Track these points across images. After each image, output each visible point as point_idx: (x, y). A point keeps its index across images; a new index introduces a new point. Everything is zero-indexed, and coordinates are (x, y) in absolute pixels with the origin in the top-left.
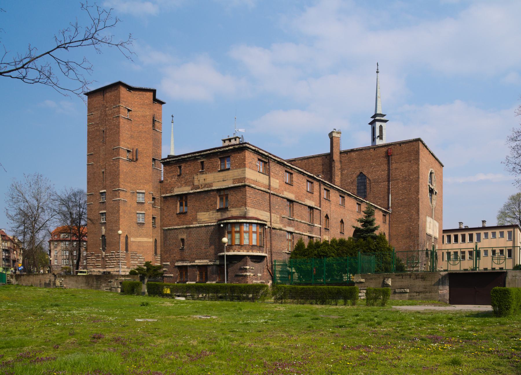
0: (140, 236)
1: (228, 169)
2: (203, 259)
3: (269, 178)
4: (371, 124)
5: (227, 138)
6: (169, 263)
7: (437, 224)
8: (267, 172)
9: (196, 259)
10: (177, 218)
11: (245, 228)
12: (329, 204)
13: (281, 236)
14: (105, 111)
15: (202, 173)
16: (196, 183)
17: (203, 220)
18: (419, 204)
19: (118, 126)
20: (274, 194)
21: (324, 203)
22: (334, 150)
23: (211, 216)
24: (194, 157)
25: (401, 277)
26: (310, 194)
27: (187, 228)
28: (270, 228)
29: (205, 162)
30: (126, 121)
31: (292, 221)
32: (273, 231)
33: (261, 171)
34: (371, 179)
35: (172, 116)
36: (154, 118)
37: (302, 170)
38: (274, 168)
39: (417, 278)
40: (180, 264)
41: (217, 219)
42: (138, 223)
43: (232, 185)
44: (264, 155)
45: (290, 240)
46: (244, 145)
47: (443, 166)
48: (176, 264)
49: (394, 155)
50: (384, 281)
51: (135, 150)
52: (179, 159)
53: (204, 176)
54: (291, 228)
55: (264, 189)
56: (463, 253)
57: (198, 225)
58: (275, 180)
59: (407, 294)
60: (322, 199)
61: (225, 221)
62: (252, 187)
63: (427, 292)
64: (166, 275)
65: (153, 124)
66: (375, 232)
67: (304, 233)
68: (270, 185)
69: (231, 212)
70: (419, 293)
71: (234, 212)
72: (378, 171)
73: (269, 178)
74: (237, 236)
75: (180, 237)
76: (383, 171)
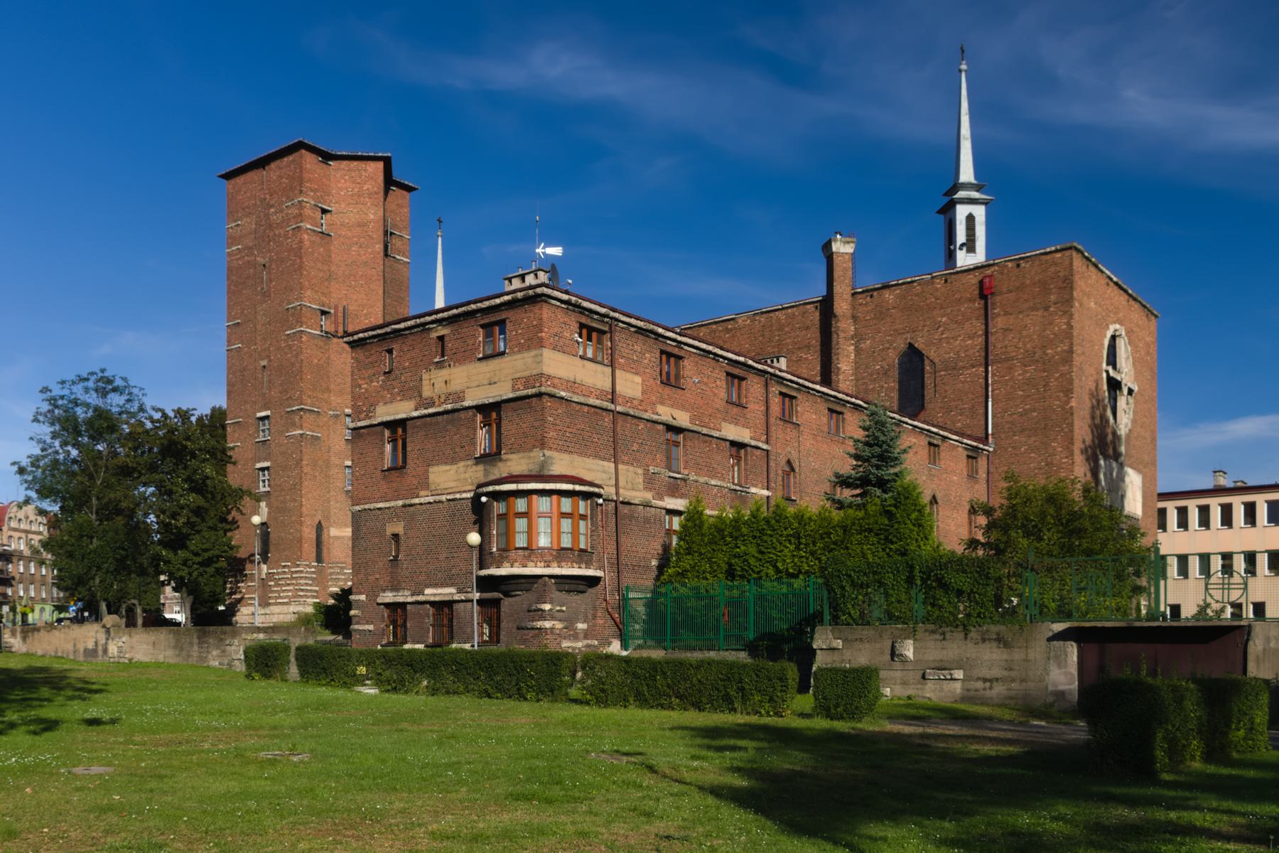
1: (503, 354)
2: (442, 585)
6: (363, 597)
10: (382, 482)
13: (647, 520)
14: (267, 216)
15: (440, 365)
16: (427, 392)
17: (442, 486)
18: (1072, 424)
19: (298, 252)
21: (778, 430)
23: (462, 476)
26: (736, 410)
27: (404, 506)
30: (317, 239)
32: (624, 510)
33: (590, 355)
34: (936, 361)
36: (385, 226)
37: (710, 348)
38: (630, 347)
39: (984, 640)
40: (388, 597)
41: (476, 482)
43: (511, 395)
44: (597, 313)
46: (539, 290)
49: (1001, 293)
50: (893, 647)
51: (341, 309)
53: (444, 373)
55: (597, 402)
56: (1227, 557)
57: (431, 499)
58: (629, 376)
61: (490, 488)
62: (562, 398)
63: (1013, 680)
70: (990, 681)
71: (516, 463)
72: (955, 338)
74: (521, 524)
75: (391, 529)
76: (970, 338)
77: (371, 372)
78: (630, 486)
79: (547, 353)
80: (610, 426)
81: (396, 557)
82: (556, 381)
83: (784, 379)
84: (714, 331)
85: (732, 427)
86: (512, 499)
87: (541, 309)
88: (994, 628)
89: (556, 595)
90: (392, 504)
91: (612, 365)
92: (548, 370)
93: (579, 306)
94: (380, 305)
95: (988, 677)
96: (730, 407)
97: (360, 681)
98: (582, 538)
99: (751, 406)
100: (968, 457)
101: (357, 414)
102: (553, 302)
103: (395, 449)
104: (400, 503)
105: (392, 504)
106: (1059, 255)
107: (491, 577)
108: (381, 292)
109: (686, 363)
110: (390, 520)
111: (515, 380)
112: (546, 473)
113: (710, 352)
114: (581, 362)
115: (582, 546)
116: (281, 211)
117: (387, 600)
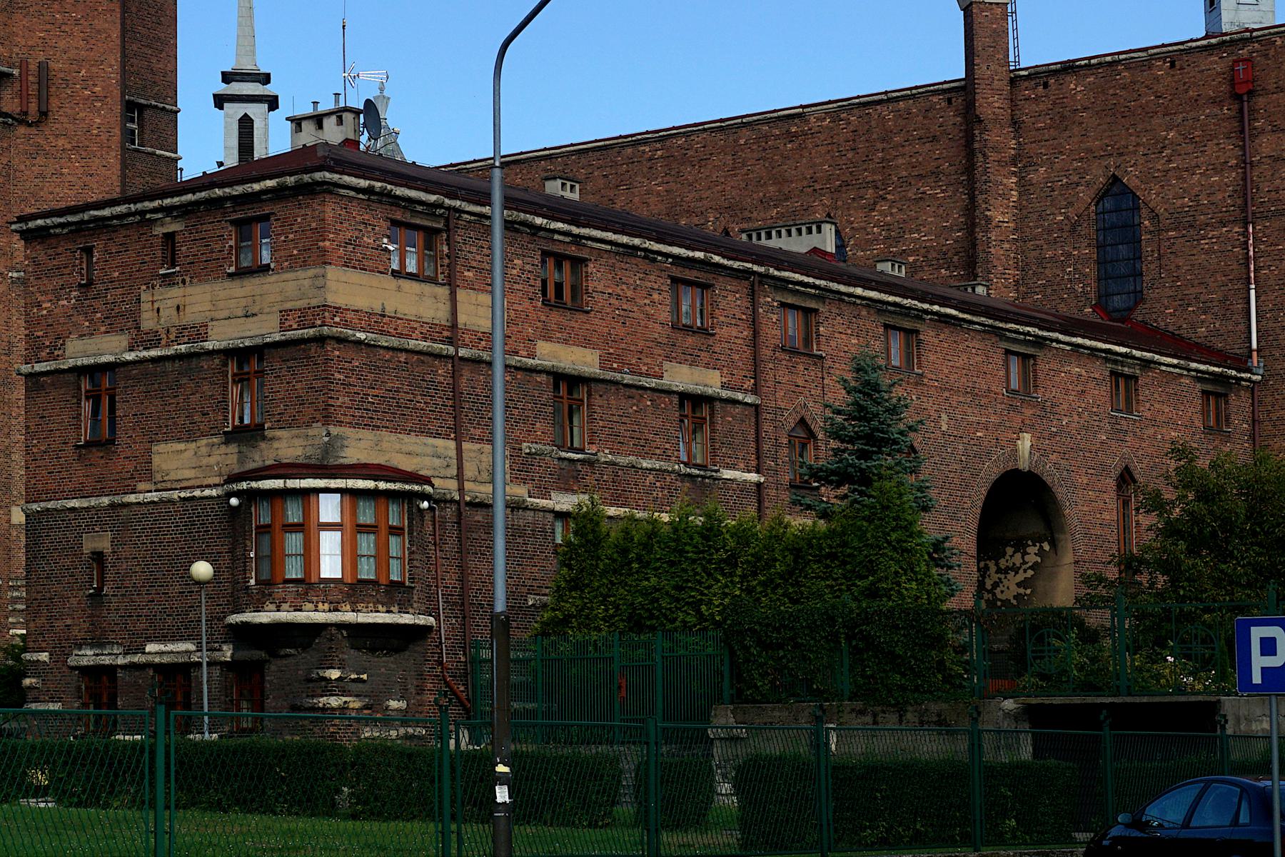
1: (265, 269)
3: (453, 295)
5: (309, 110)
6: (44, 656)
9: (150, 639)
12: (814, 372)
15: (168, 281)
17: (173, 476)
21: (779, 373)
22: (982, 70)
23: (205, 461)
24: (137, 213)
27: (112, 506)
33: (411, 267)
40: (87, 657)
41: (225, 470)
43: (277, 337)
49: (1266, 92)
51: (33, 67)
52: (82, 222)
53: (175, 294)
55: (423, 345)
57: (154, 496)
61: (244, 485)
64: (33, 706)
68: (454, 326)
69: (276, 445)
72: (1191, 170)
73: (453, 295)
74: (294, 542)
77: (56, 282)
79: (332, 272)
80: (442, 382)
81: (100, 589)
82: (350, 315)
84: (766, 137)
85: (685, 369)
86: (278, 503)
87: (323, 203)
88: (934, 707)
89: (350, 655)
90: (93, 502)
91: (452, 284)
92: (334, 299)
93: (389, 195)
94: (114, 60)
96: (679, 335)
98: (395, 566)
99: (722, 332)
101: (34, 350)
102: (342, 191)
103: (95, 412)
104: (106, 501)
105: (93, 502)
107: (246, 625)
108: (115, 34)
109: (591, 267)
110: (90, 528)
111: (285, 313)
112: (332, 462)
114: (391, 283)
115: (394, 577)
117: (84, 662)
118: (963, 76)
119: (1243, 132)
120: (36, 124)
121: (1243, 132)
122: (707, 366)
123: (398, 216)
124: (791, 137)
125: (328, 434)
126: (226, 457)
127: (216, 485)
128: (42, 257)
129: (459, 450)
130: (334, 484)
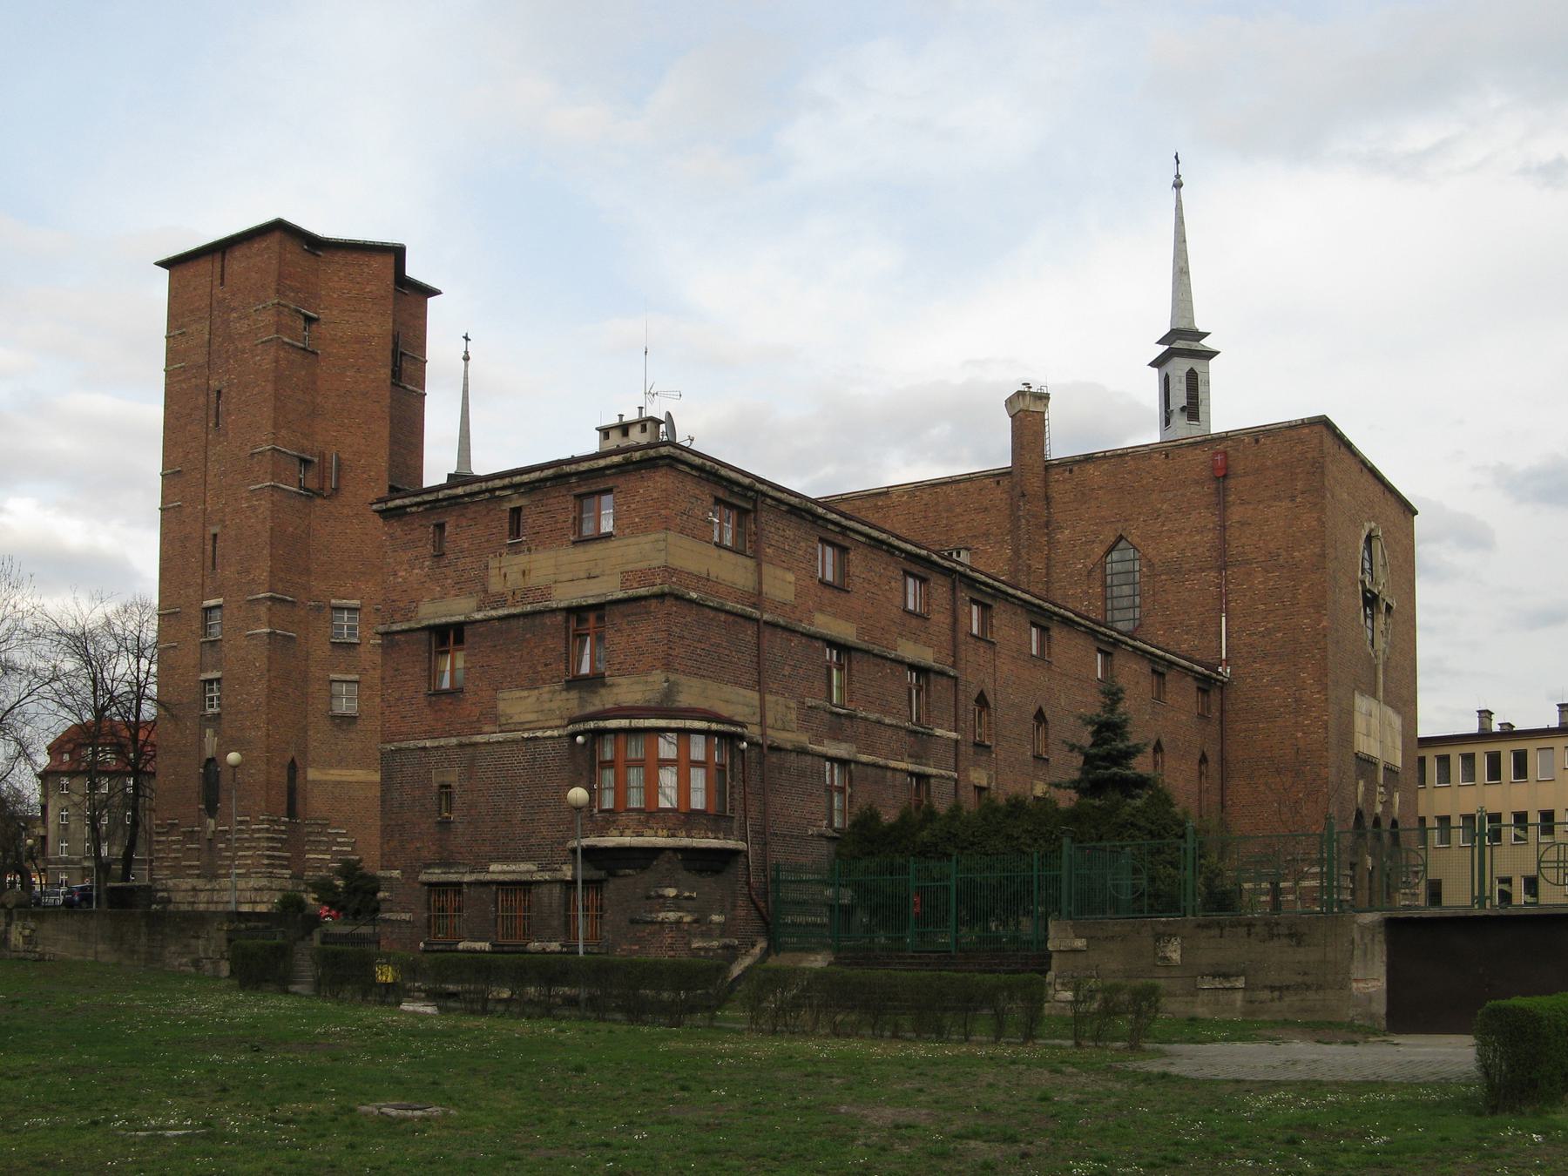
0: (341, 763)
3: (759, 565)
4: (1157, 363)
6: (396, 873)
7: (1397, 721)
8: (748, 546)
10: (427, 711)
11: (667, 749)
15: (515, 549)
16: (495, 585)
17: (516, 719)
18: (1325, 650)
20: (774, 625)
23: (547, 706)
25: (1216, 932)
27: (461, 745)
28: (761, 746)
29: (525, 512)
31: (847, 723)
32: (774, 758)
33: (728, 541)
35: (466, 338)
36: (396, 344)
38: (779, 532)
39: (1272, 937)
40: (436, 875)
42: (334, 717)
43: (620, 595)
44: (739, 484)
45: (842, 790)
47: (1416, 513)
48: (423, 877)
53: (522, 560)
54: (844, 745)
57: (499, 737)
58: (779, 572)
59: (1239, 996)
60: (961, 636)
61: (592, 725)
63: (1308, 988)
64: (387, 916)
65: (395, 364)
66: (1133, 762)
67: (893, 764)
68: (760, 593)
69: (615, 690)
70: (1280, 989)
73: (759, 565)
78: (780, 723)
83: (976, 581)
90: (442, 742)
91: (757, 557)
95: (1277, 984)
97: (392, 994)
100: (1199, 689)
104: (454, 741)
105: (442, 742)
106: (1306, 431)
108: (386, 433)
113: (882, 542)
114: (716, 552)
116: (247, 317)
117: (434, 879)
118: (1007, 463)
119: (1221, 502)
120: (328, 497)
121: (1221, 502)
122: (925, 644)
123: (720, 494)
124: (877, 508)
125: (667, 680)
126: (569, 702)
127: (557, 727)
128: (399, 533)
129: (762, 700)
130: (674, 724)
